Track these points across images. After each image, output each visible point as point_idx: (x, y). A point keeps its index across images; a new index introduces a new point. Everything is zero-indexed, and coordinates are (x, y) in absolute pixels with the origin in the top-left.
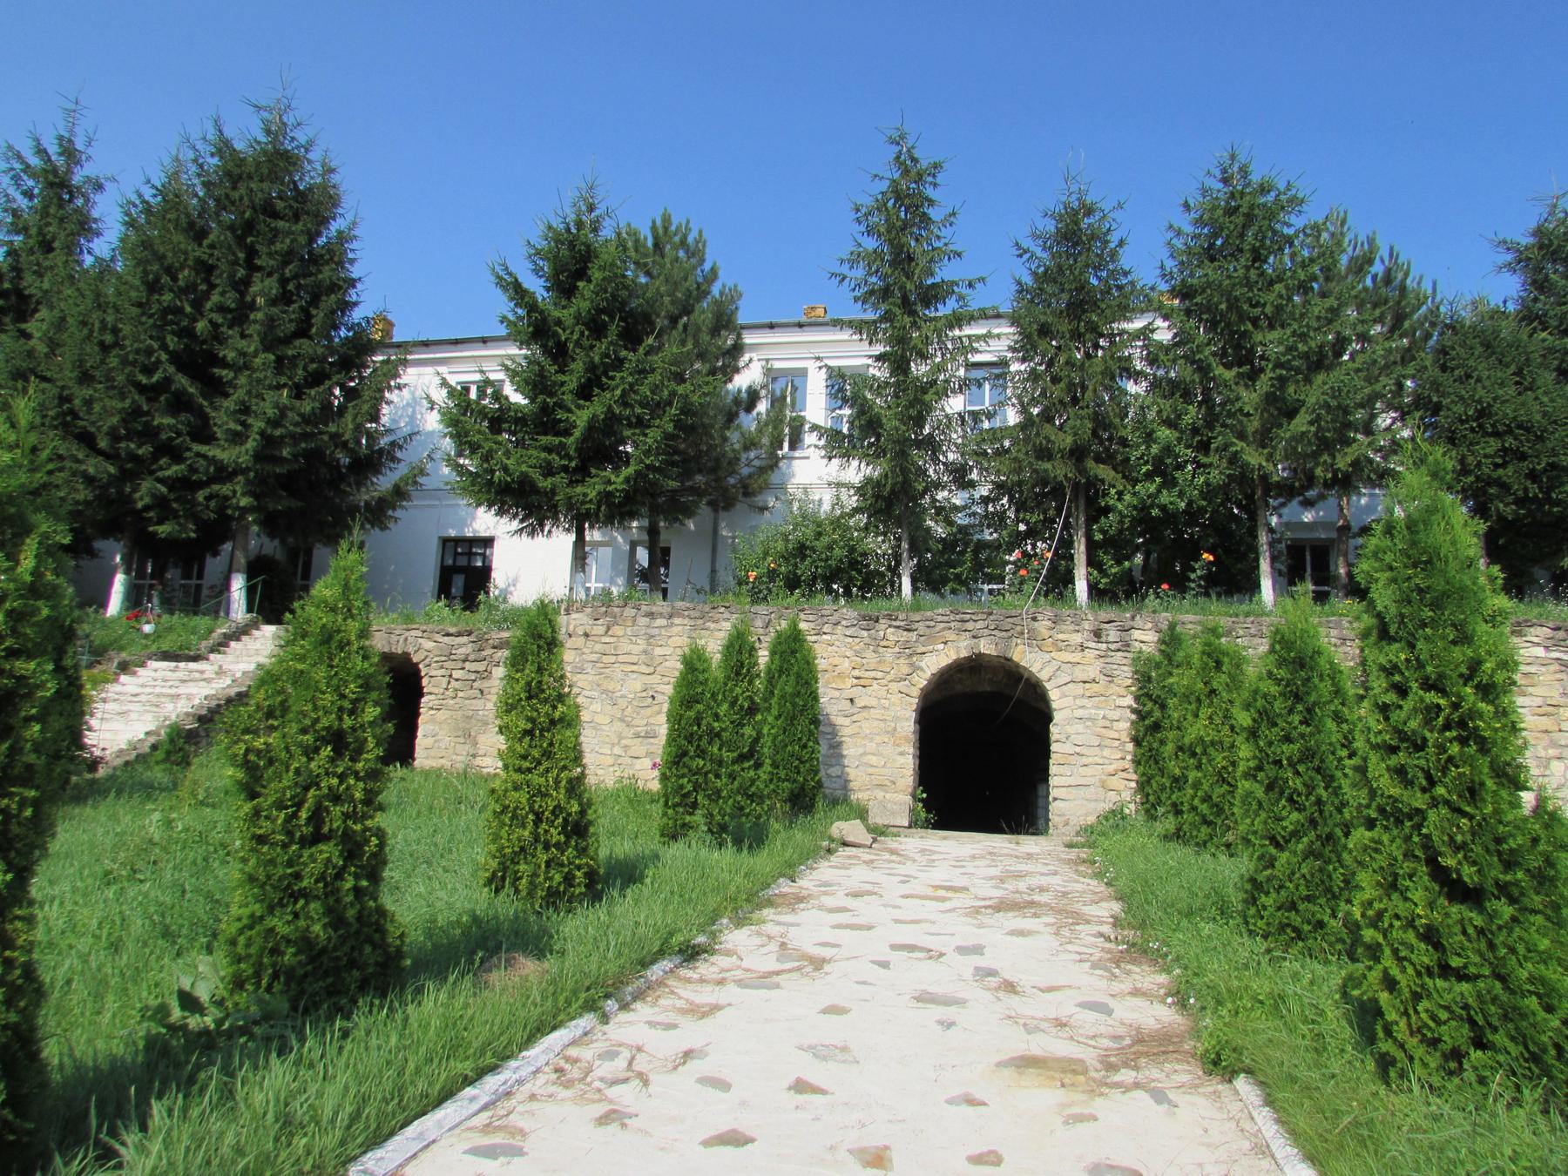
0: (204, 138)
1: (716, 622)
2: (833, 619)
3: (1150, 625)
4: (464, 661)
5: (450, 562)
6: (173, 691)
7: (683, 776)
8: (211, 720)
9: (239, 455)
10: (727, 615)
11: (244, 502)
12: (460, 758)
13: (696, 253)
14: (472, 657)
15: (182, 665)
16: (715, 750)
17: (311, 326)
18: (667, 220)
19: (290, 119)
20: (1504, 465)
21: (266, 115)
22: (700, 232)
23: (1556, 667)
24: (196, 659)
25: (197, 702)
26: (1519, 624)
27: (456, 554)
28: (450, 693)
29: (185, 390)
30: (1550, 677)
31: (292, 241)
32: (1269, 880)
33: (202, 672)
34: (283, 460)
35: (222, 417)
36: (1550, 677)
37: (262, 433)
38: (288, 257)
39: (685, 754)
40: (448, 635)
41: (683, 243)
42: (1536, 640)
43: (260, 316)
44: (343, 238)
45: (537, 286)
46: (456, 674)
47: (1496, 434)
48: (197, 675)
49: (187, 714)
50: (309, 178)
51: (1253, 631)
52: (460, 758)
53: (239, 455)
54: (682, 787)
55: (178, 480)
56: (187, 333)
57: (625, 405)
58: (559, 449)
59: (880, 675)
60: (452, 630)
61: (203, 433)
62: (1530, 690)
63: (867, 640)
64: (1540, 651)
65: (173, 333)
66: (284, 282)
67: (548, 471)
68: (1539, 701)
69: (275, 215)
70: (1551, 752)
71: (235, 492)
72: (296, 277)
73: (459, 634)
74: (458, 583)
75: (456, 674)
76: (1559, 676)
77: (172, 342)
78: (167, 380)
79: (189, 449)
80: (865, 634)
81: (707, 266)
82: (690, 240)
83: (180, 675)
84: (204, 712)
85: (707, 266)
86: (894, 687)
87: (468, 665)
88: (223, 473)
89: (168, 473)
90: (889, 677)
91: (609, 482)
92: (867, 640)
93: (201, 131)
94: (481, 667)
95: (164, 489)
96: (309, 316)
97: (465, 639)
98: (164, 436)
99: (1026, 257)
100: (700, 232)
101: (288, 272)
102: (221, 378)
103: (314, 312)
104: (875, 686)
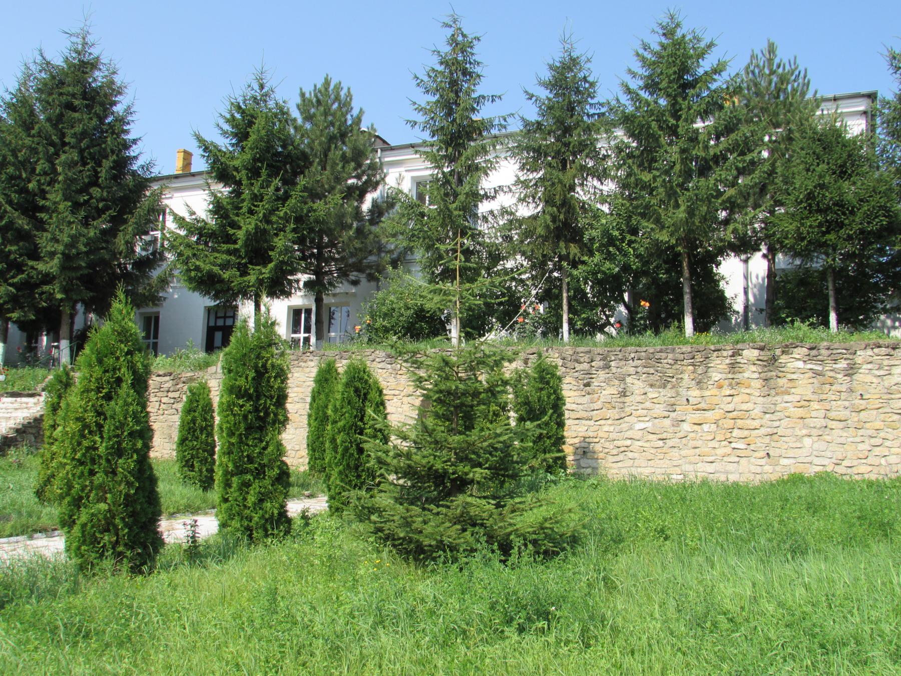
0: (35, 62)
1: (305, 362)
2: (371, 358)
3: (557, 355)
4: (168, 391)
5: (212, 324)
6: (9, 415)
7: (185, 451)
8: (24, 432)
9: (51, 266)
10: (311, 358)
11: (59, 296)
12: (165, 452)
13: (346, 105)
14: (171, 389)
15: (19, 399)
16: (204, 436)
17: (98, 178)
18: (327, 83)
19: (90, 39)
20: (828, 232)
21: (74, 39)
22: (349, 89)
23: (810, 374)
24: (32, 395)
25: (18, 421)
26: (787, 346)
27: (217, 318)
28: (161, 412)
29: (22, 227)
30: (805, 381)
31: (84, 125)
32: (108, 461)
33: (27, 403)
34: (79, 268)
35: (44, 241)
36: (805, 381)
37: (63, 254)
38: (84, 134)
39: (187, 439)
40: (159, 376)
41: (337, 98)
42: (798, 357)
43: (61, 178)
44: (128, 111)
45: (224, 143)
46: (164, 400)
47: (819, 211)
48: (25, 405)
49: (10, 428)
50: (98, 78)
51: (620, 357)
52: (165, 452)
53: (51, 266)
54: (185, 457)
55: (22, 283)
56: (24, 191)
57: (268, 222)
58: (235, 252)
59: (397, 392)
60: (161, 373)
61: (35, 254)
62: (793, 390)
63: (390, 371)
64: (800, 364)
65: (15, 192)
66: (81, 152)
67: (225, 266)
68: (798, 398)
69: (74, 109)
70: (804, 432)
71: (54, 290)
72: (88, 147)
73: (165, 375)
74: (218, 336)
75: (164, 400)
76: (811, 381)
77: (14, 197)
78: (11, 223)
79: (27, 265)
80: (389, 366)
81: (355, 112)
82: (343, 94)
83: (16, 405)
84: (20, 427)
85: (355, 112)
86: (405, 399)
87: (170, 394)
88: (48, 279)
89: (15, 280)
90: (402, 394)
91: (261, 273)
92: (390, 371)
93: (31, 57)
94: (176, 395)
95: (13, 290)
96: (96, 172)
97: (167, 378)
98: (12, 257)
99: (534, 99)
100: (349, 89)
101: (83, 145)
102: (42, 219)
103: (99, 170)
104: (395, 400)
